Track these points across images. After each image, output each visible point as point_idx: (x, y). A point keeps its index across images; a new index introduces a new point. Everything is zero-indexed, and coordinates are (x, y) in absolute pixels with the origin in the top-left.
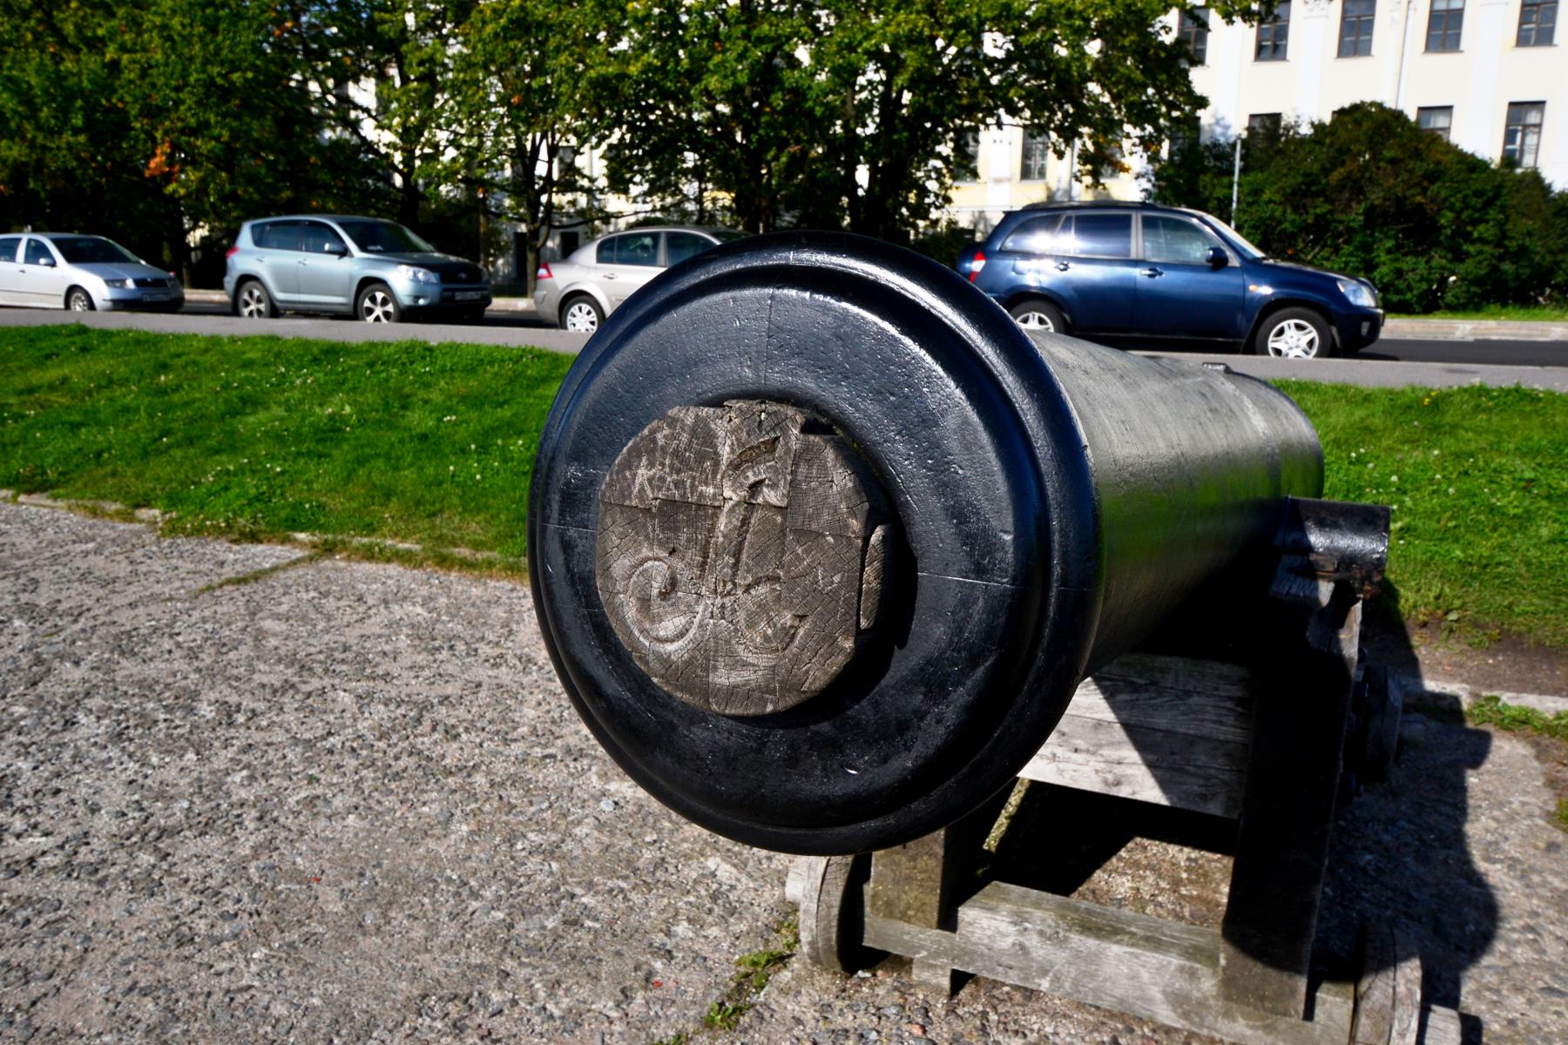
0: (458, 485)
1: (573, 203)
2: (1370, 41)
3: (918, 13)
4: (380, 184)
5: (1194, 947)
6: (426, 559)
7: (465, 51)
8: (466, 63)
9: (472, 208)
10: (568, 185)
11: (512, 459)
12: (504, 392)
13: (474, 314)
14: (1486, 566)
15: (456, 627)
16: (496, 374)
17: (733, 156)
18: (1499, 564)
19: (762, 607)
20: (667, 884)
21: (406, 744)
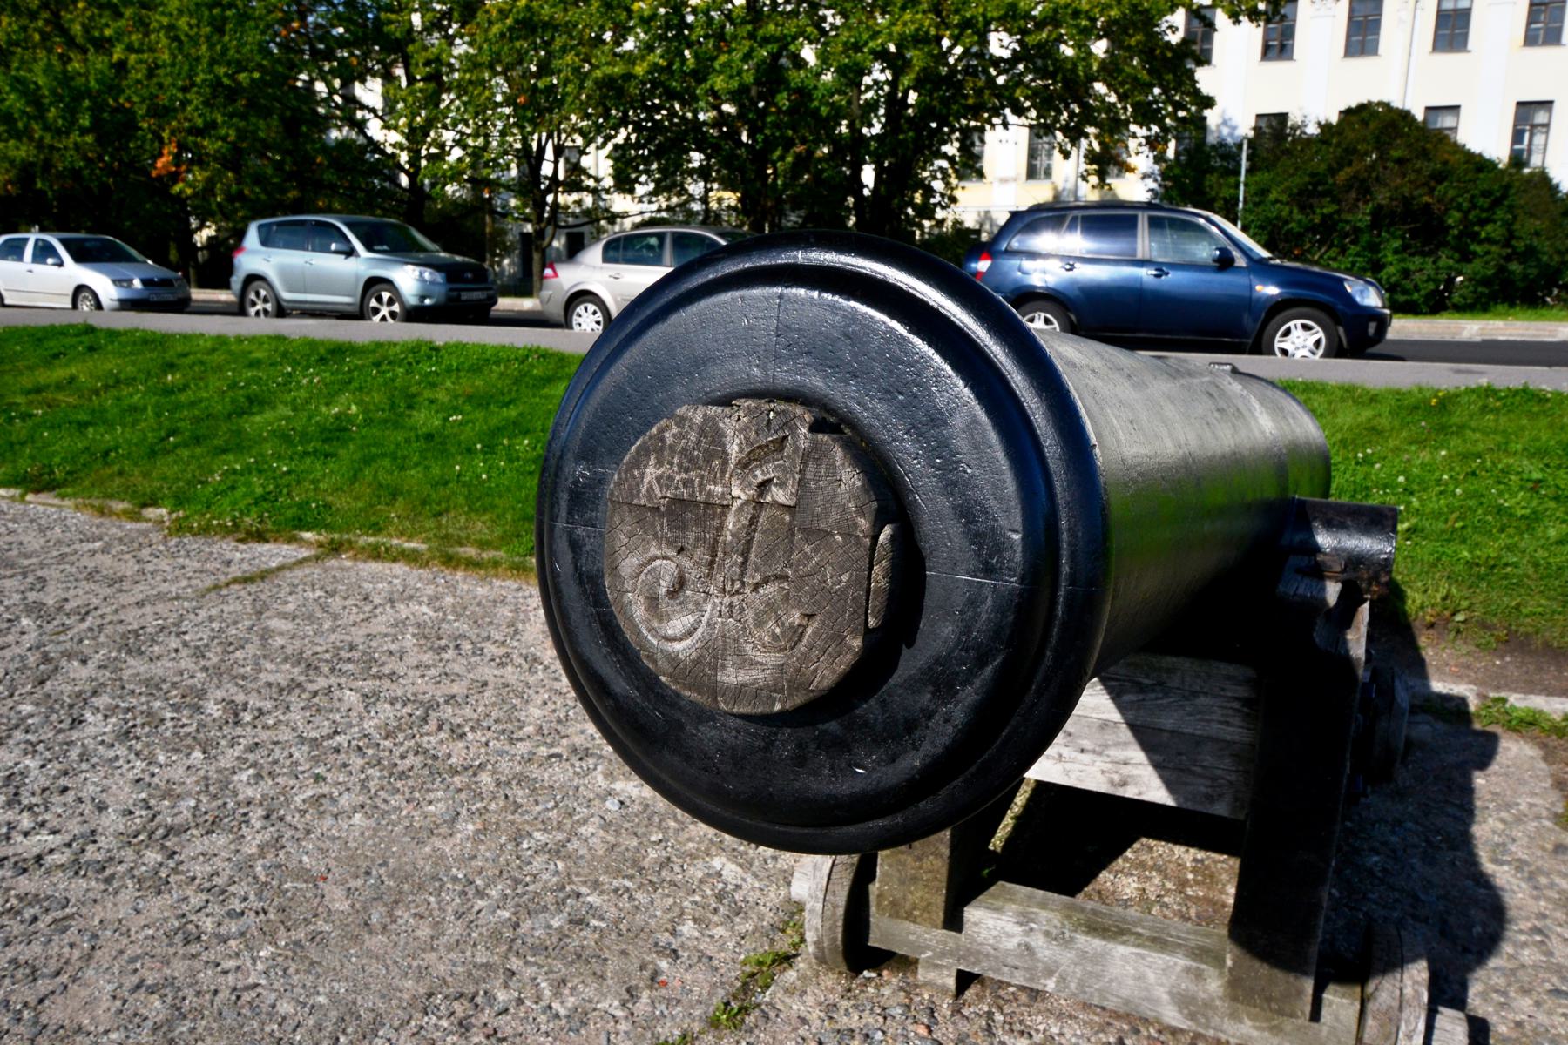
0: (464, 484)
1: (579, 203)
2: (1377, 42)
3: (924, 12)
4: (387, 184)
5: (1200, 948)
6: (433, 558)
7: (471, 51)
8: (472, 63)
9: (478, 208)
10: (573, 186)
11: (518, 459)
12: (510, 392)
13: (480, 314)
14: (1494, 567)
15: (462, 626)
16: (502, 374)
17: (738, 157)
18: (1506, 565)
19: (770, 606)
20: (673, 883)
21: (412, 743)
